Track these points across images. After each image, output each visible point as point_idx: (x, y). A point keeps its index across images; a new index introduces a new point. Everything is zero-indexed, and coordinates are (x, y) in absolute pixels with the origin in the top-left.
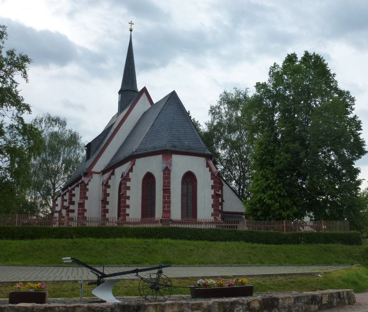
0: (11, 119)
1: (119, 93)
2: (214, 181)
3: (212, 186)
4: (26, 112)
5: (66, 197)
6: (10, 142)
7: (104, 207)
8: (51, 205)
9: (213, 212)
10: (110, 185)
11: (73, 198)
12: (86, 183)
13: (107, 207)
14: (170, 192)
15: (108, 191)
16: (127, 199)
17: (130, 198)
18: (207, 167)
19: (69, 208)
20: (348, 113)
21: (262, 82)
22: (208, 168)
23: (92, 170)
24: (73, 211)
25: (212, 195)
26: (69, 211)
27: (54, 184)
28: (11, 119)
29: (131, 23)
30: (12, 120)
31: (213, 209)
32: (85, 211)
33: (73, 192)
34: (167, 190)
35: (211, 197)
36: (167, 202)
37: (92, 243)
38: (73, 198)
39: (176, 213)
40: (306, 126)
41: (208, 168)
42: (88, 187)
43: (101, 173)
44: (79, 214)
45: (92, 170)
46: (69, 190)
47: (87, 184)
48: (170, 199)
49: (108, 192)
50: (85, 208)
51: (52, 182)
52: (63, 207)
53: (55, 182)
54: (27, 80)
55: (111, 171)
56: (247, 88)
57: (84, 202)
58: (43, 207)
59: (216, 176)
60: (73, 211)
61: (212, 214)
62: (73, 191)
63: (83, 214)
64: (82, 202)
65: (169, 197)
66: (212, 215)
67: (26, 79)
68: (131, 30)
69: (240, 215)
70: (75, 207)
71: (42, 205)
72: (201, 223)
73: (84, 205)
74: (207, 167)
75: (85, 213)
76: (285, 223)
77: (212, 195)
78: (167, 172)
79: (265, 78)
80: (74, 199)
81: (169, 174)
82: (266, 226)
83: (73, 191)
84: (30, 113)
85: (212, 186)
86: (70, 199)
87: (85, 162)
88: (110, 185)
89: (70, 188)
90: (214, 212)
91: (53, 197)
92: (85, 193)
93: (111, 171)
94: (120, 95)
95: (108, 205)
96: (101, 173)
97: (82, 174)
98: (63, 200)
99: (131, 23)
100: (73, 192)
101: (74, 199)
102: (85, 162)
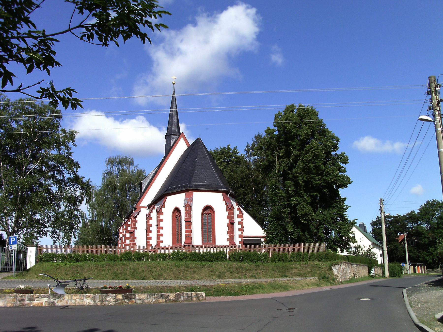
1: (165, 137)
7: (147, 235)
13: (162, 232)
17: (164, 228)
23: (140, 205)
32: (136, 238)
34: (188, 221)
36: (189, 231)
37: (418, 303)
39: (197, 240)
40: (109, 241)
42: (136, 219)
45: (140, 205)
47: (136, 217)
50: (135, 236)
57: (134, 231)
63: (134, 241)
65: (190, 227)
69: (260, 238)
72: (218, 247)
73: (134, 234)
76: (270, 247)
78: (188, 207)
79: (270, 124)
82: (276, 248)
92: (135, 225)
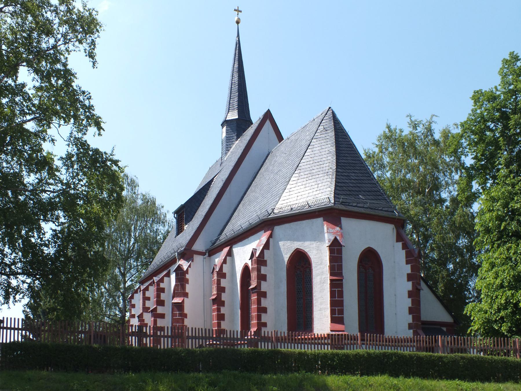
0: (67, 143)
2: (411, 266)
3: (408, 275)
4: (92, 130)
5: (152, 292)
6: (68, 185)
8: (121, 305)
9: (411, 321)
10: (225, 274)
11: (162, 294)
12: (185, 270)
13: (223, 310)
14: (342, 284)
15: (224, 283)
16: (263, 297)
18: (398, 240)
19: (156, 311)
20: (28, 305)
21: (486, 88)
22: (400, 244)
24: (162, 316)
25: (409, 292)
26: (157, 316)
27: (124, 275)
28: (67, 143)
29: (238, 11)
30: (69, 145)
31: (411, 316)
32: (185, 316)
33: (162, 285)
35: (407, 295)
38: (162, 294)
41: (400, 244)
43: (207, 254)
44: (174, 321)
46: (155, 281)
48: (343, 297)
49: (222, 285)
51: (120, 271)
52: (145, 309)
53: (124, 272)
54: (94, 64)
55: (226, 250)
56: (434, 115)
58: (110, 309)
59: (415, 256)
60: (162, 316)
61: (410, 325)
62: (161, 283)
64: (180, 302)
66: (410, 327)
67: (91, 60)
68: (238, 22)
69: (439, 327)
70: (166, 310)
71: (109, 306)
74: (398, 240)
75: (185, 319)
77: (409, 292)
80: (163, 296)
81: (340, 252)
83: (161, 283)
84: (99, 134)
85: (408, 275)
86: (158, 296)
87: (175, 237)
88: (225, 274)
89: (156, 279)
90: (413, 321)
91: (123, 294)
92: (184, 288)
93: (226, 250)
94: (225, 127)
95: (223, 307)
96: (207, 254)
97: (176, 255)
98: (146, 299)
99: (238, 11)
100: (162, 285)
101: (163, 296)
102: (175, 237)
